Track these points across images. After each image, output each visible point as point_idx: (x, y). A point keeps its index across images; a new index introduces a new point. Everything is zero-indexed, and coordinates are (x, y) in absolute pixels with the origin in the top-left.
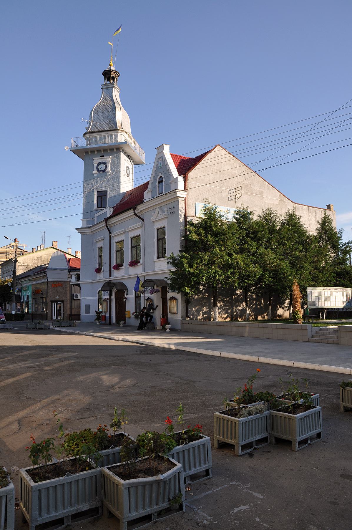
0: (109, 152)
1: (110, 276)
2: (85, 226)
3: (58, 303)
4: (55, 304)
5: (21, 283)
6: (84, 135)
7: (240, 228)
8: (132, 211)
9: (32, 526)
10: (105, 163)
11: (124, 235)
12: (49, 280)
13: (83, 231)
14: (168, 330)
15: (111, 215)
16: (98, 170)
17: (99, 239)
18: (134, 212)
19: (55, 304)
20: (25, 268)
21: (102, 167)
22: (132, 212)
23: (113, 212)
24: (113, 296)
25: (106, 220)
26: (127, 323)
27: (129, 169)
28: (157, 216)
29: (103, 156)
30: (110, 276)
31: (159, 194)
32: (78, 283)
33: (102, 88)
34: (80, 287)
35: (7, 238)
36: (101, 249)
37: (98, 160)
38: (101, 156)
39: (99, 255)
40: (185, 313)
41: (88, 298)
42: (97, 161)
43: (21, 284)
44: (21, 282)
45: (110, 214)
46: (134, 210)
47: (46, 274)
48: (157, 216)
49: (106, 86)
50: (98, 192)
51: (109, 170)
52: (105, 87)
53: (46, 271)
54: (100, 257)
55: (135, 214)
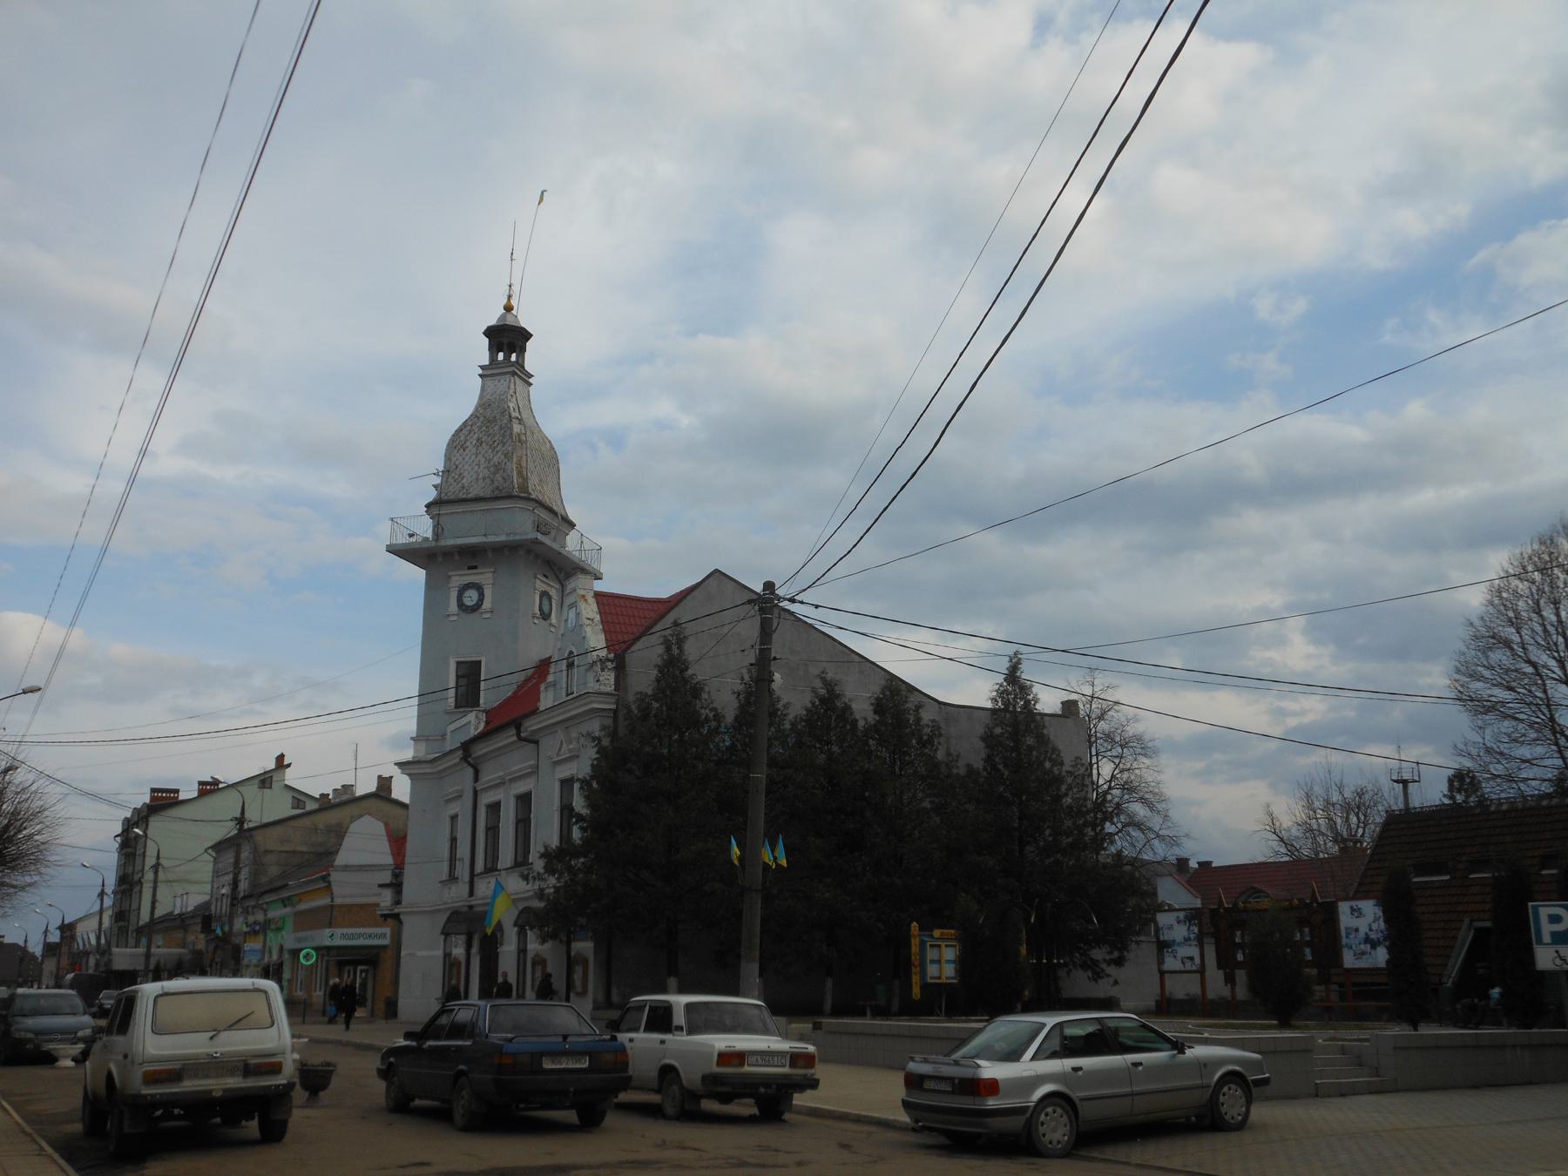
0: (440, 559)
1: (471, 893)
2: (422, 754)
3: (359, 968)
4: (349, 972)
5: (265, 906)
6: (428, 506)
7: (1548, 648)
8: (513, 731)
9: (20, 720)
10: (479, 588)
11: (501, 790)
12: (338, 901)
13: (416, 770)
14: (774, 1086)
15: (479, 731)
16: (461, 604)
17: (489, 781)
18: (518, 734)
19: (349, 972)
20: (1503, 582)
21: (471, 597)
22: (511, 733)
23: (487, 723)
24: (475, 950)
25: (466, 747)
26: (131, 968)
27: (550, 598)
28: (560, 750)
29: (475, 567)
30: (471, 893)
31: (568, 695)
32: (396, 911)
33: (480, 375)
34: (401, 922)
35: (539, 204)
36: (454, 818)
37: (462, 578)
38: (470, 568)
39: (1046, 718)
40: (601, 997)
41: (419, 954)
42: (459, 579)
43: (265, 911)
44: (267, 903)
45: (476, 729)
46: (518, 728)
47: (329, 882)
48: (560, 750)
49: (492, 369)
50: (458, 663)
51: (487, 604)
52: (489, 372)
53: (329, 875)
54: (453, 840)
55: (520, 739)
